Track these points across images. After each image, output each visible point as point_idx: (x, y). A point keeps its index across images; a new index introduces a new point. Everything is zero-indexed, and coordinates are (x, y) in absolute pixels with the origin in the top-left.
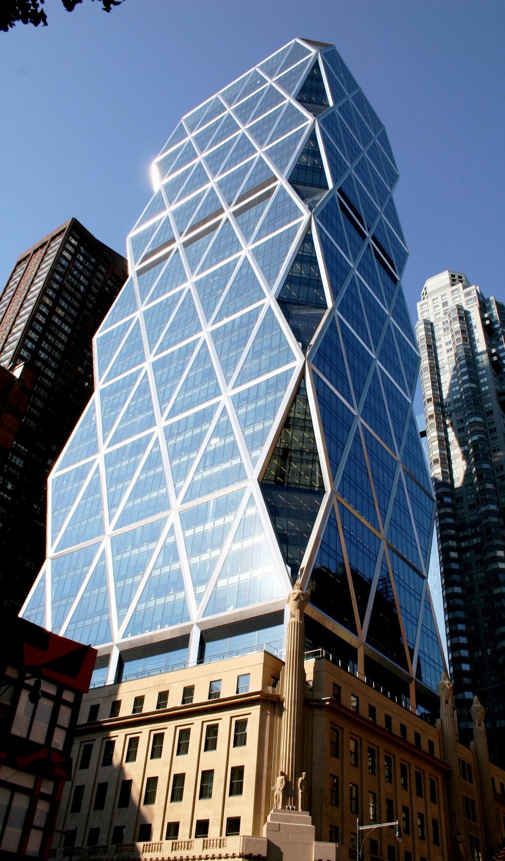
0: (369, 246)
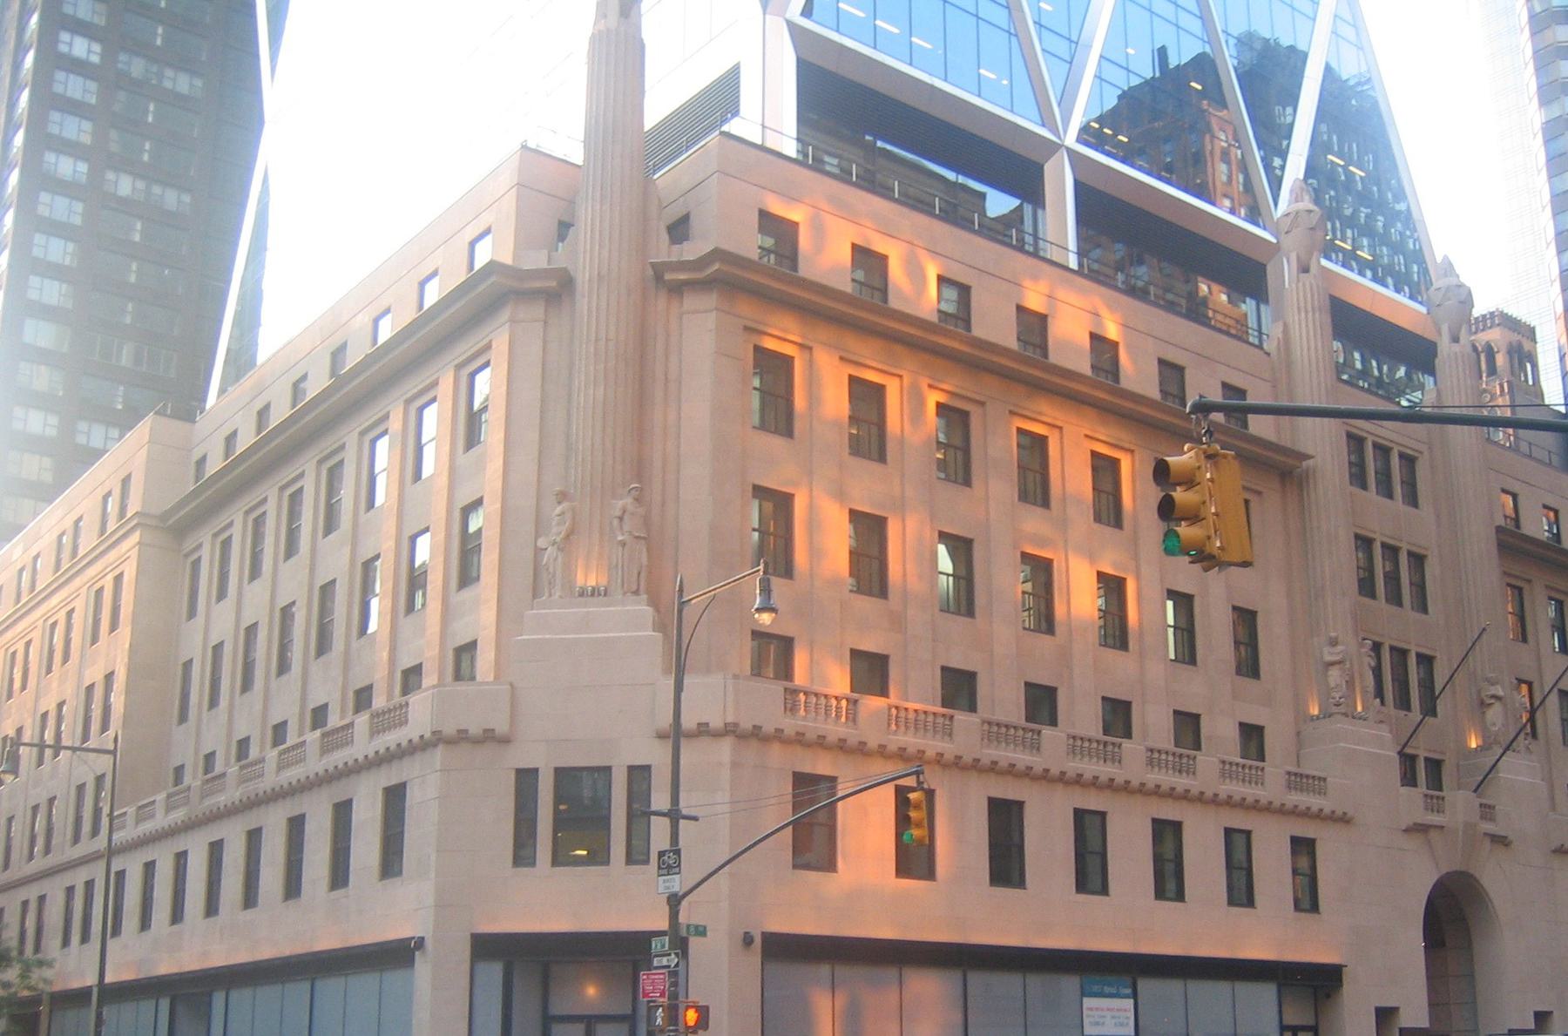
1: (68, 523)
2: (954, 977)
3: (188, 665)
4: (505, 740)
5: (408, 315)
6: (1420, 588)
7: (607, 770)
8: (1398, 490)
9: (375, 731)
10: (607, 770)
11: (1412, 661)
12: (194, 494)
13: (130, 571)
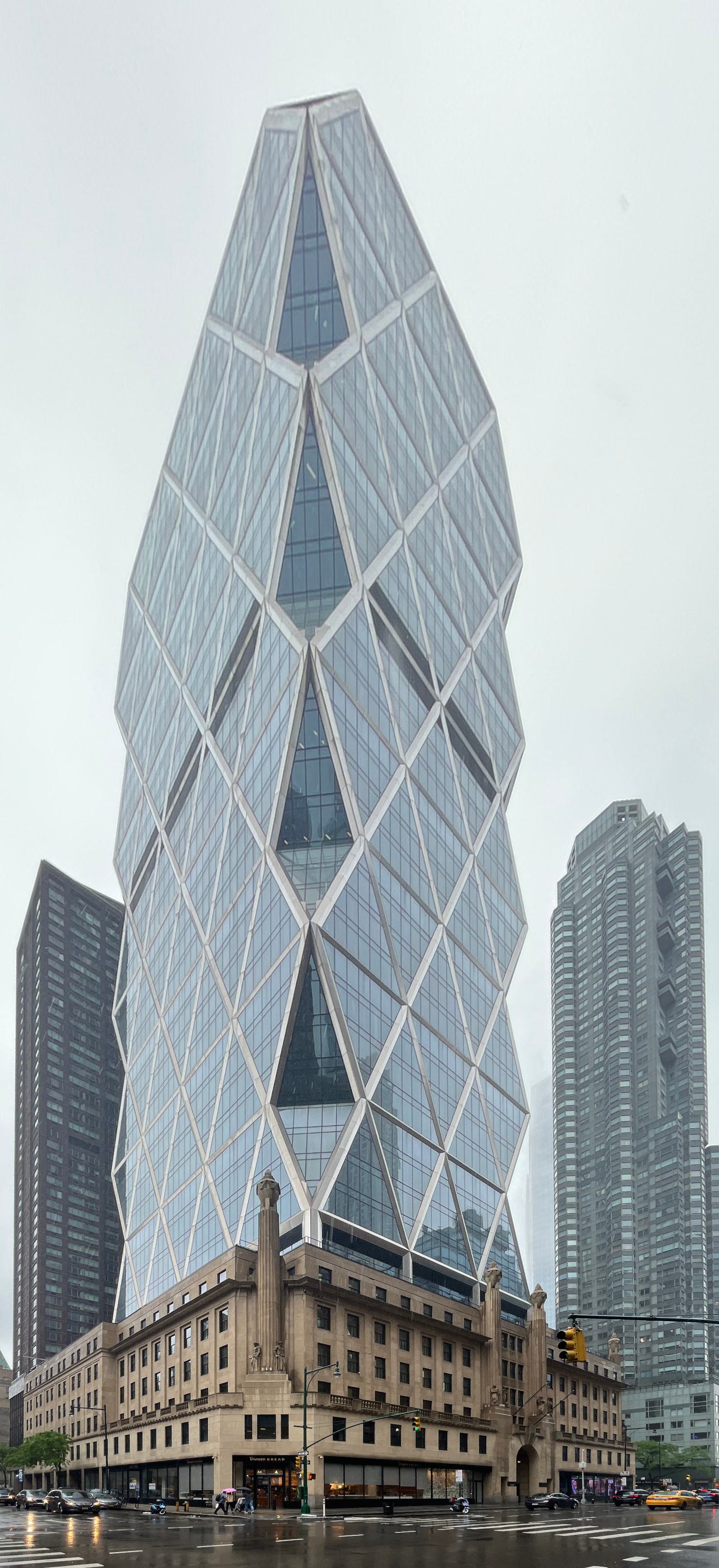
0: (439, 722)
1: (75, 1351)
2: (412, 1472)
3: (122, 1389)
4: (241, 1408)
5: (165, 1314)
6: (520, 1374)
7: (274, 1416)
8: (516, 1348)
9: (162, 1414)
10: (274, 1416)
11: (517, 1393)
12: (119, 1344)
13: (100, 1364)
